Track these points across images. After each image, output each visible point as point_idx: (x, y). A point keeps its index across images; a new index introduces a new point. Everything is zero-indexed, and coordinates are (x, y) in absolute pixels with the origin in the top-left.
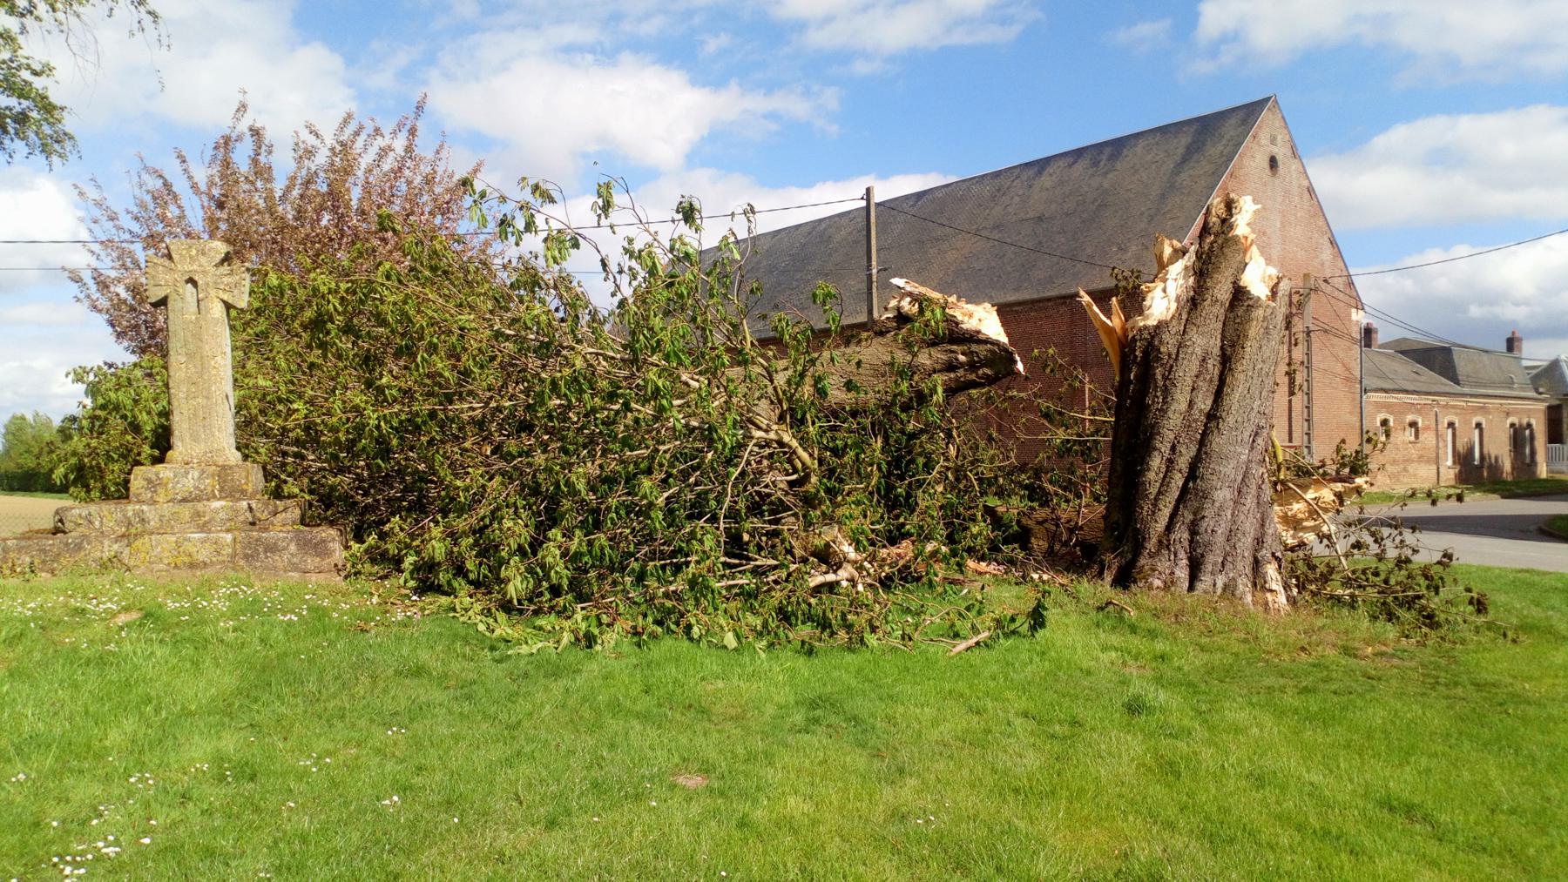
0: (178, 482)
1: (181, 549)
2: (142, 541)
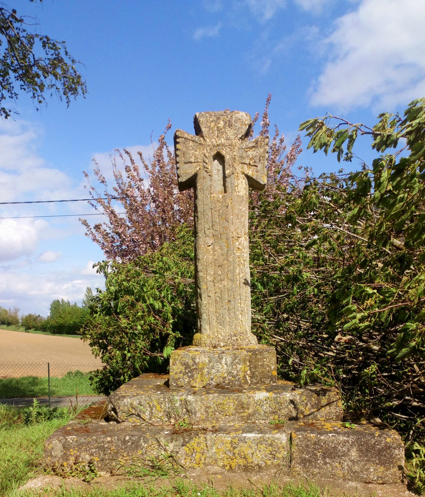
0: (213, 368)
1: (236, 451)
2: (197, 440)
